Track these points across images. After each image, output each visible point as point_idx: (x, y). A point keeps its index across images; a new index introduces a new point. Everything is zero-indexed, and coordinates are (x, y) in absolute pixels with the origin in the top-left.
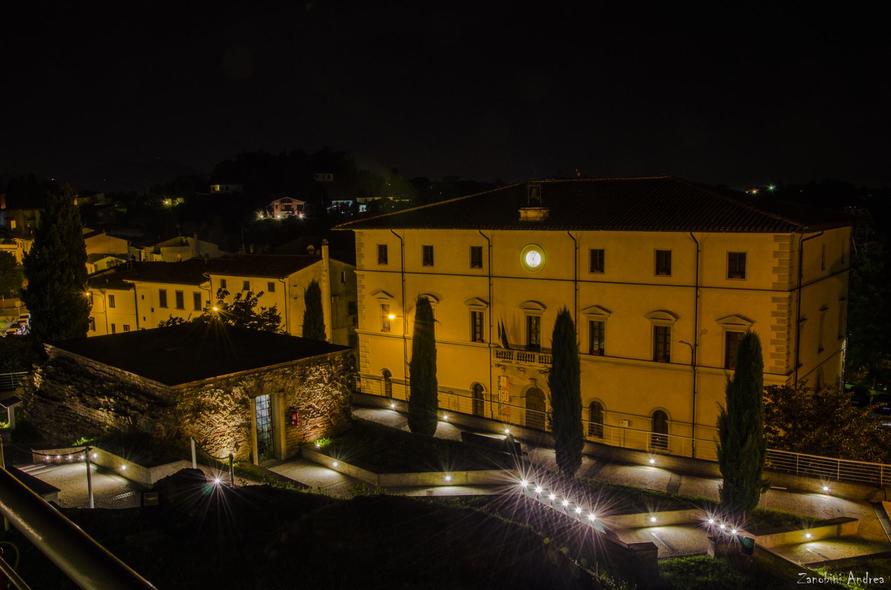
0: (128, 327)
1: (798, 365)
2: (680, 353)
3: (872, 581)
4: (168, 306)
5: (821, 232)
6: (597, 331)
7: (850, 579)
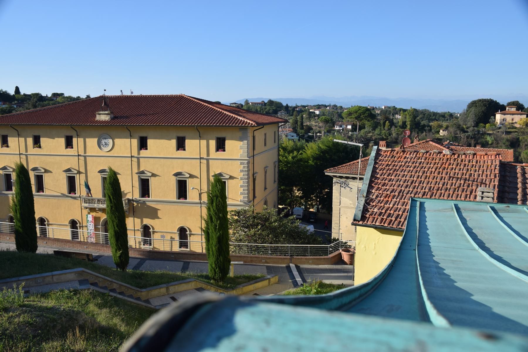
1: (254, 197)
2: (81, 190)
4: (9, 145)
5: (262, 126)
6: (39, 179)
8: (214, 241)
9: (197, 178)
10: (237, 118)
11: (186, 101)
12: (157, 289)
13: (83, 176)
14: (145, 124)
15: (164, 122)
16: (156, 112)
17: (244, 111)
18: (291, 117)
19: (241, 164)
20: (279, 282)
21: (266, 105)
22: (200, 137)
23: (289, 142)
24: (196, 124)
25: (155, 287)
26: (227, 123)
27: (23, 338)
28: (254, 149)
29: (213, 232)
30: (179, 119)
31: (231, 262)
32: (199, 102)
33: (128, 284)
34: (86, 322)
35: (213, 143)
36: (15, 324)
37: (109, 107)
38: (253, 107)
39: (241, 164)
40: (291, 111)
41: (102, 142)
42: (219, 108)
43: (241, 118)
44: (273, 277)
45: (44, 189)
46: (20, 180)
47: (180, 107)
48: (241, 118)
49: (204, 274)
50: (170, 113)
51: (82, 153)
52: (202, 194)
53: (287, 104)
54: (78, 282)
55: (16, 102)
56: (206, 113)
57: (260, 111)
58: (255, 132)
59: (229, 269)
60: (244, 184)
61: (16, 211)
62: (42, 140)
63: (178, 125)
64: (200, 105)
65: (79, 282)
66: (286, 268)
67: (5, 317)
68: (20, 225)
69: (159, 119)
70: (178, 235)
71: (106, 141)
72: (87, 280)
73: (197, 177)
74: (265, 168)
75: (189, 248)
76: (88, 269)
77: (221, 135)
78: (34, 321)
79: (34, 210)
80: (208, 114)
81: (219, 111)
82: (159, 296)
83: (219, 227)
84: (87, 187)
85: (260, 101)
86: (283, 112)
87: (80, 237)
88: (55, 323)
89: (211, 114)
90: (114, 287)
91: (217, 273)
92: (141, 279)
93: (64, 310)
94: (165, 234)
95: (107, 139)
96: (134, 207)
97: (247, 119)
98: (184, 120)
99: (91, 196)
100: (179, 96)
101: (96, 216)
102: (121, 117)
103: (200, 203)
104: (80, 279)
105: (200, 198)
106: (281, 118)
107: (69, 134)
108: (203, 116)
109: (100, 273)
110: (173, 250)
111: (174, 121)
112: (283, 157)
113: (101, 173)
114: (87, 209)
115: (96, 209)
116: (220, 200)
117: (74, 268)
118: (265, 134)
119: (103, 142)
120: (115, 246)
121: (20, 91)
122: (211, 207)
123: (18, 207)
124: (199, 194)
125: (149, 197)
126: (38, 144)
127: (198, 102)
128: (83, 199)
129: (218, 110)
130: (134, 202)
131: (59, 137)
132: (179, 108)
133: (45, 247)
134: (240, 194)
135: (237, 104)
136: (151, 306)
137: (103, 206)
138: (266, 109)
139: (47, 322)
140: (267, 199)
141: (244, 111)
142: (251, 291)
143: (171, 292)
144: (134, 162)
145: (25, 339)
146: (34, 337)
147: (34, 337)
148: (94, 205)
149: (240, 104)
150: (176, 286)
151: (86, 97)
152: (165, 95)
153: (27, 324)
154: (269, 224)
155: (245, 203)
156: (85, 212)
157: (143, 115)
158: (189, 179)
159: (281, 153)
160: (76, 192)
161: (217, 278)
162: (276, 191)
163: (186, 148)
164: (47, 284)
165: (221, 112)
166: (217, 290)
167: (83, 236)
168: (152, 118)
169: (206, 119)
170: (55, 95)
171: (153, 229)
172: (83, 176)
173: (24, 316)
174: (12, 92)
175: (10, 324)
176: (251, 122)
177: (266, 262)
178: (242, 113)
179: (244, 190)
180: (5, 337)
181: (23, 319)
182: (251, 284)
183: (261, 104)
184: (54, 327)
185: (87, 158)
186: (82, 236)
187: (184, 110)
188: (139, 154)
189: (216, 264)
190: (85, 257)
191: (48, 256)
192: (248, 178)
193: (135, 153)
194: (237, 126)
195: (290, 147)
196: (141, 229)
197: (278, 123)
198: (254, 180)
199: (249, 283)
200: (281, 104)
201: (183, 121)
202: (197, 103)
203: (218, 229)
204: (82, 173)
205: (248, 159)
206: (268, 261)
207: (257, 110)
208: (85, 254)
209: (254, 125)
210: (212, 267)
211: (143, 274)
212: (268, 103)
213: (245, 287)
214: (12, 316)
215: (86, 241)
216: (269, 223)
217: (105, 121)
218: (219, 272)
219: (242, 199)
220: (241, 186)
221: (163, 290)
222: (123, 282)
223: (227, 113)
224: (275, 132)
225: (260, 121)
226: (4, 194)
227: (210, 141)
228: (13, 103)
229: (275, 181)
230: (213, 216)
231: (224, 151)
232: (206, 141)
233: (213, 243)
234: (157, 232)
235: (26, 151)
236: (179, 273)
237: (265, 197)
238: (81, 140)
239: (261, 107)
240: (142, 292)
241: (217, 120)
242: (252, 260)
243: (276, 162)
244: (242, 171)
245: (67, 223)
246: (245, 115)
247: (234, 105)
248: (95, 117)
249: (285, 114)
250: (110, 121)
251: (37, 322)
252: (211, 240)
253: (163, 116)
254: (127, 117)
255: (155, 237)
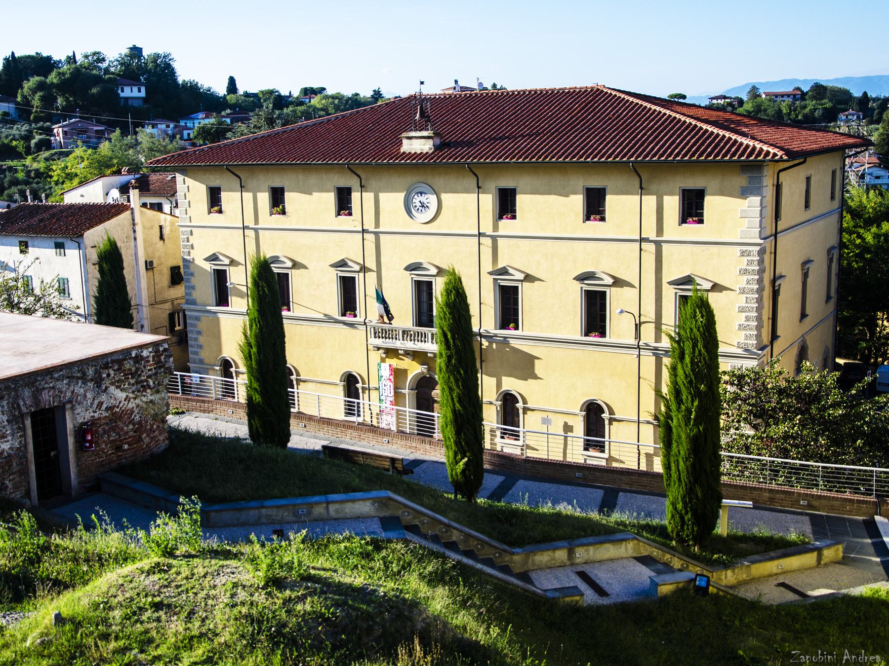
0: (30, 278)
1: (774, 336)
3: (868, 659)
5: (802, 160)
7: (845, 657)
8: (681, 448)
9: (633, 286)
10: (736, 141)
11: (608, 102)
12: (548, 550)
13: (371, 277)
14: (510, 160)
15: (556, 154)
16: (537, 131)
17: (752, 122)
18: (877, 126)
19: (743, 254)
20: (845, 561)
21: (807, 97)
22: (641, 188)
23: (868, 193)
24: (631, 156)
25: (542, 546)
26: (709, 155)
27: (315, 647)
28: (777, 216)
29: (680, 426)
30: (592, 146)
31: (724, 501)
32: (640, 102)
33: (482, 533)
34: (428, 624)
35: (672, 204)
36: (297, 616)
37: (429, 121)
38: (772, 104)
39: (743, 254)
40: (876, 112)
41: (414, 200)
42: (689, 116)
43: (745, 141)
44: (828, 546)
45: (291, 303)
46: (258, 291)
47: (593, 117)
48: (745, 141)
49: (656, 522)
50: (570, 131)
51: (370, 225)
52: (643, 326)
53: (865, 94)
54: (379, 522)
55: (228, 111)
56: (657, 129)
57: (789, 114)
58: (781, 174)
59: (716, 516)
60: (749, 305)
61: (250, 356)
62: (288, 196)
63: (589, 160)
64: (643, 110)
65: (382, 523)
66: (863, 526)
67: (278, 598)
68: (257, 387)
69: (545, 146)
70: (582, 419)
71: (423, 198)
72: (397, 519)
73: (630, 285)
74: (804, 264)
75: (607, 451)
76: (399, 494)
77: (694, 182)
78: (332, 614)
79: (285, 357)
80: (662, 131)
81: (690, 124)
82: (550, 568)
83: (696, 416)
84: (381, 300)
85: (789, 89)
86: (853, 115)
87: (364, 412)
88: (371, 623)
89: (669, 131)
90: (454, 539)
91: (688, 525)
92: (511, 525)
93: (385, 595)
94: (551, 415)
95: (425, 194)
96: (483, 351)
97: (761, 141)
98: (603, 148)
99: (388, 322)
100: (592, 90)
101: (398, 367)
102: (457, 144)
103: (638, 346)
104: (382, 514)
105: (638, 336)
106: (849, 135)
107: (343, 183)
108: (649, 136)
109: (422, 505)
110: (568, 460)
111: (579, 151)
112: (850, 235)
113: (411, 271)
114: (381, 351)
115: (400, 351)
116: (703, 351)
117: (371, 490)
118: (808, 179)
119: (417, 200)
120: (453, 445)
121: (238, 86)
122: (679, 366)
123: (254, 350)
124: (636, 325)
125: (516, 328)
126: (281, 207)
127: (637, 104)
128: (372, 329)
129: (688, 120)
130: (483, 339)
131: (322, 191)
132: (590, 119)
133: (301, 435)
134: (737, 328)
135: (728, 98)
136: (535, 589)
137: (414, 346)
138: (805, 107)
139: (356, 619)
140: (808, 342)
141: (752, 122)
142: (770, 576)
143: (578, 561)
144: (486, 248)
145: (319, 650)
146: (335, 648)
147: (335, 648)
148: (395, 343)
149: (735, 98)
150: (591, 548)
151: (372, 93)
152: (558, 87)
153: (320, 618)
154: (820, 410)
155: (746, 350)
156: (376, 356)
157: (506, 138)
158: (613, 289)
159: (845, 225)
160: (358, 312)
161: (687, 536)
162: (831, 321)
163: (608, 215)
164: (316, 520)
165: (696, 126)
166: (687, 566)
167: (370, 409)
168: (528, 144)
169: (656, 145)
170: (309, 92)
171: (525, 402)
172: (371, 277)
173: (313, 601)
174: (221, 90)
175: (289, 615)
176: (772, 150)
177: (810, 506)
178: (747, 126)
179: (747, 319)
180: (284, 639)
181: (312, 607)
182: (772, 559)
183: (792, 97)
184: (370, 630)
185: (382, 236)
186: (367, 410)
187: (604, 124)
188: (496, 228)
189: (684, 503)
190: (387, 464)
191: (312, 454)
192: (760, 290)
193: (487, 228)
194: (735, 161)
195: (872, 207)
196: (497, 400)
197: (842, 148)
198: (775, 294)
199: (767, 557)
200: (847, 93)
201: (600, 151)
202: (635, 106)
203: (695, 419)
204: (371, 270)
205: (762, 241)
206: (815, 503)
207: (780, 110)
208: (387, 457)
209: (781, 157)
210: (675, 508)
211: (516, 513)
212: (810, 93)
213: (757, 565)
214: (290, 597)
215: (375, 423)
216: (817, 408)
217: (421, 153)
218: (693, 523)
219: (742, 341)
220: (742, 310)
221: (561, 555)
222: (472, 529)
223: (710, 128)
224: (834, 173)
225: (795, 146)
226: (210, 312)
227: (666, 199)
228: (223, 113)
229: (829, 298)
230: (683, 389)
231: (701, 221)
232: (654, 197)
233: (679, 453)
234: (533, 410)
235: (256, 221)
236: (594, 515)
237: (803, 336)
238: (369, 197)
239: (794, 103)
240: (513, 554)
241: (684, 147)
242: (772, 499)
243: (833, 248)
244: (745, 272)
245: (337, 379)
246: (755, 131)
247: (719, 101)
248: (400, 144)
249: (858, 118)
250: (433, 153)
251: (337, 617)
252: (674, 445)
253: (554, 138)
254: (470, 144)
255: (529, 422)
